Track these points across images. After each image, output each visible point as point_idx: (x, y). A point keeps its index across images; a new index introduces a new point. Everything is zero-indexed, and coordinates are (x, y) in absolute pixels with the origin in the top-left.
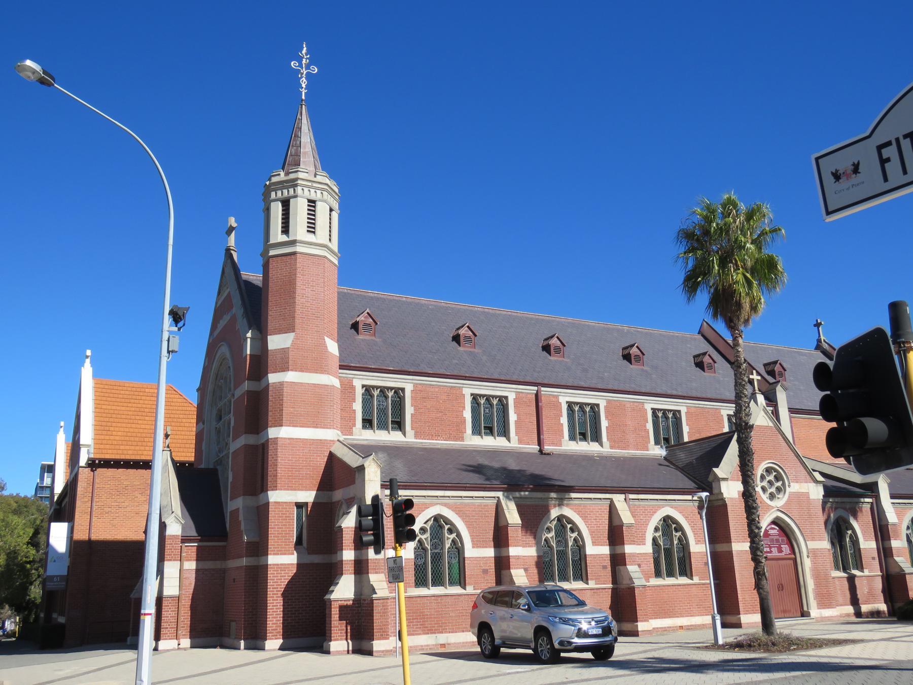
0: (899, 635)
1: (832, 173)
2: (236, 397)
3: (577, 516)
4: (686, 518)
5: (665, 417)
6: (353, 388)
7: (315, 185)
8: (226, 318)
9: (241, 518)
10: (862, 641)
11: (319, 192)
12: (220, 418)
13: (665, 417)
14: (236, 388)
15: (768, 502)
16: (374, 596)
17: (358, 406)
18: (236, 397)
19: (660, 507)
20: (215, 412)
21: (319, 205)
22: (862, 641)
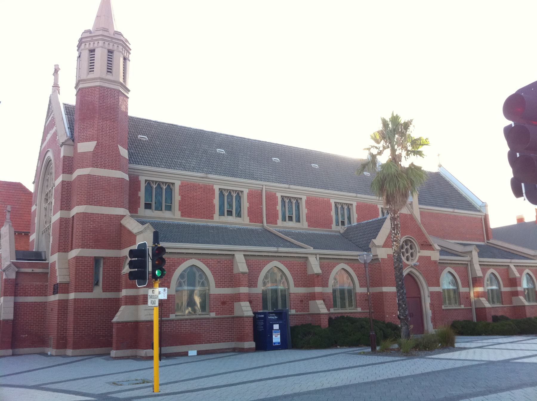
0: (486, 344)
1: (372, 138)
2: (56, 185)
3: (208, 269)
4: (354, 271)
5: (343, 208)
6: (139, 182)
7: (114, 41)
8: (52, 132)
9: (57, 267)
10: (465, 349)
11: (116, 45)
12: (47, 200)
13: (343, 208)
14: (55, 180)
15: (405, 261)
16: (513, 125)
17: (142, 194)
18: (56, 185)
19: (338, 264)
20: (44, 197)
21: (116, 54)
22: (465, 349)
